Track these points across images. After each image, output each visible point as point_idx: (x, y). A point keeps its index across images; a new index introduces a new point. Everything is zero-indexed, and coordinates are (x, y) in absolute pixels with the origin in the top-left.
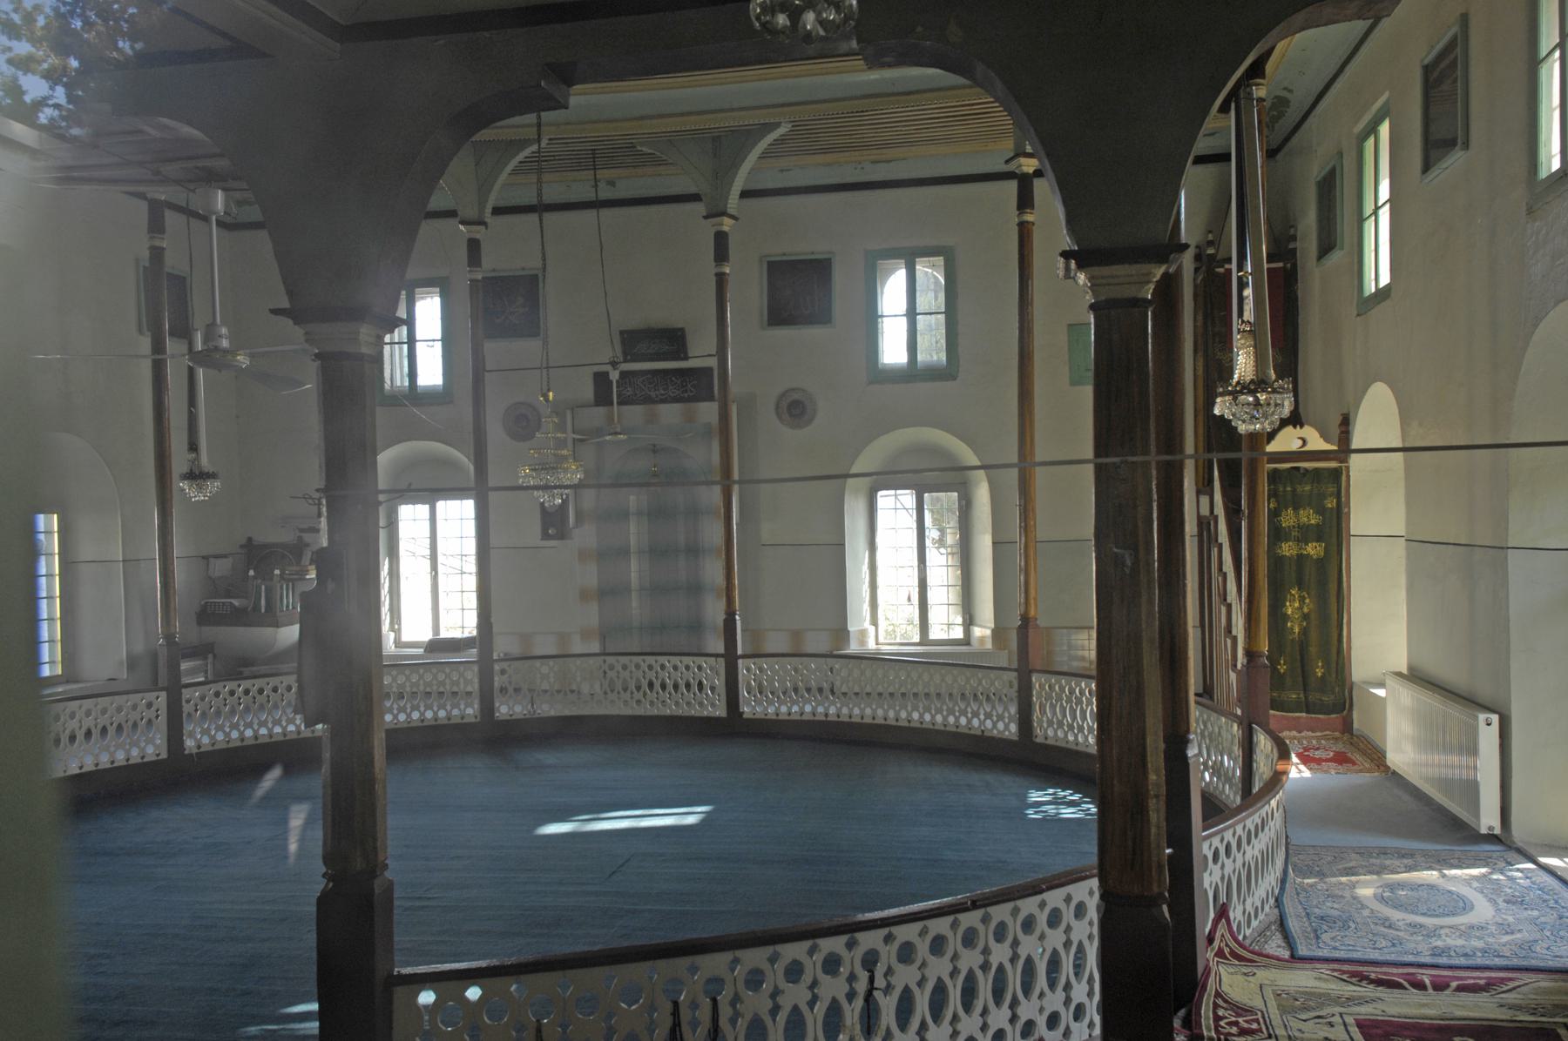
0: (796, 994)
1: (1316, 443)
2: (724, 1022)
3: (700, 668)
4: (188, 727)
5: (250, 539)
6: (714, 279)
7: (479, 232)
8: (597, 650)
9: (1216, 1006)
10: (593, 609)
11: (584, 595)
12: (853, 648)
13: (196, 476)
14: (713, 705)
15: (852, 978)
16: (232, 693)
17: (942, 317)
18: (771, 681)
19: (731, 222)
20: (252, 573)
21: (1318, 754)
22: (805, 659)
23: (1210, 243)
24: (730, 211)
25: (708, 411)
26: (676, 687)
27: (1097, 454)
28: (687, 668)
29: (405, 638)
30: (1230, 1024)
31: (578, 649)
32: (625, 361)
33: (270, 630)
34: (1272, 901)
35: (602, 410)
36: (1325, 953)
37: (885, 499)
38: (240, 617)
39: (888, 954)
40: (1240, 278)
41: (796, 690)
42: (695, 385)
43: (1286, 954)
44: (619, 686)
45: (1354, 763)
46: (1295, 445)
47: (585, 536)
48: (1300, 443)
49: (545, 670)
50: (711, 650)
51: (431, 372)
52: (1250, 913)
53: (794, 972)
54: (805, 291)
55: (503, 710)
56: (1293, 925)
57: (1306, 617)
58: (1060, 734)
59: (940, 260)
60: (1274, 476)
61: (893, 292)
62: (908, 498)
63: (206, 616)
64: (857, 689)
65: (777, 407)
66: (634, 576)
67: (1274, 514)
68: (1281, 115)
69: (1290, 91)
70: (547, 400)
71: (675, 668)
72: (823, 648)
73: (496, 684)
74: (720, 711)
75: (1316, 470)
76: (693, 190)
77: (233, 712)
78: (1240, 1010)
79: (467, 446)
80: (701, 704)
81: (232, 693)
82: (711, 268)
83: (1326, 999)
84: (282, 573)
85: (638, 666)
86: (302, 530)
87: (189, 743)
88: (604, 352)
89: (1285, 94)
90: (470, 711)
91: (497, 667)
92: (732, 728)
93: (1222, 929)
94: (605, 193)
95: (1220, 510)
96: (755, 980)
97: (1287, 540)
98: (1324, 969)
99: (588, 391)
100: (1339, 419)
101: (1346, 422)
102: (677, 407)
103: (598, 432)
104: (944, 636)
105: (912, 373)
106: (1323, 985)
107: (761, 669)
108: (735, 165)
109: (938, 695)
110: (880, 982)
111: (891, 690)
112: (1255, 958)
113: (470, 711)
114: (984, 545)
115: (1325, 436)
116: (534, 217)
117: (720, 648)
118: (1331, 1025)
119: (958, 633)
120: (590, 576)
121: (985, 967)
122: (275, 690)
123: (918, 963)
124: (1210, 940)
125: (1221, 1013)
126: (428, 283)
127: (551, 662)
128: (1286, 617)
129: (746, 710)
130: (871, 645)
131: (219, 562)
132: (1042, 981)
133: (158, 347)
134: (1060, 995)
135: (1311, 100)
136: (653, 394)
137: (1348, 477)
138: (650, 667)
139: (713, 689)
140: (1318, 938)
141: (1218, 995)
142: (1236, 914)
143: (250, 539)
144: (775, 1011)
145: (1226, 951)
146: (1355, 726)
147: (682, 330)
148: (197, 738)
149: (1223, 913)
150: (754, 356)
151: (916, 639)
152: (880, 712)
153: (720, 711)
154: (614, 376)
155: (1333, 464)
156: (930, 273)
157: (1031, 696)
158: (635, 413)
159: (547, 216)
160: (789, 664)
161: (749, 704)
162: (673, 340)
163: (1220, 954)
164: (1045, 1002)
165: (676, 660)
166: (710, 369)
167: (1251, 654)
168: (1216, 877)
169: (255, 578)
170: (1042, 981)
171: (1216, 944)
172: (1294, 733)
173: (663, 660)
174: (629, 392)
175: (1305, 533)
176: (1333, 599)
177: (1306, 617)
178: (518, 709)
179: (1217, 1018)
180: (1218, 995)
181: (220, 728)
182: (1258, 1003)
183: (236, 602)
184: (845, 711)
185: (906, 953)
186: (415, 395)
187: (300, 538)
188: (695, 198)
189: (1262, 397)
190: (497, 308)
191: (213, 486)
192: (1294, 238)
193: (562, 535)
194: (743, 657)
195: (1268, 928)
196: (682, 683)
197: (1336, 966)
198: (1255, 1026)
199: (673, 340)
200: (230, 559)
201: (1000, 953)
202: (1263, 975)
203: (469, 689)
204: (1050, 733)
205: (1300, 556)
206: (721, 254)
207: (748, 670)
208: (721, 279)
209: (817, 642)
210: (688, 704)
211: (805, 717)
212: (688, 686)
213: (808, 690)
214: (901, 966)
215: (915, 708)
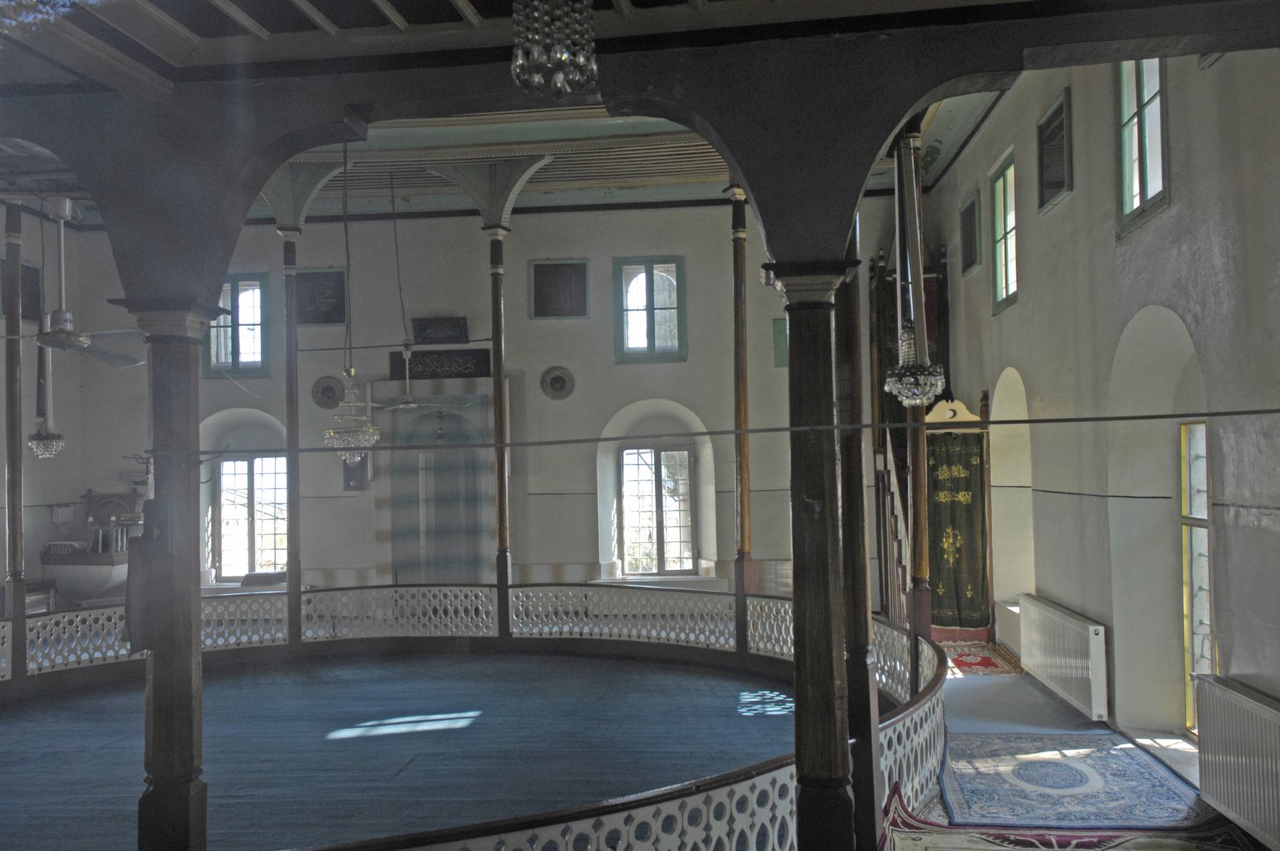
1: (965, 415)
3: (476, 596)
4: (31, 652)
5: (90, 491)
6: (490, 281)
7: (294, 237)
8: (548, 580)
10: (388, 547)
11: (380, 537)
12: (604, 578)
13: (43, 437)
14: (487, 627)
18: (535, 606)
20: (91, 519)
21: (969, 659)
22: (563, 588)
23: (881, 258)
24: (503, 224)
25: (485, 385)
26: (456, 612)
27: (793, 423)
28: (466, 596)
32: (417, 343)
33: (105, 569)
34: (934, 779)
35: (396, 383)
41: (556, 613)
42: (482, 363)
44: (419, 612)
45: (997, 666)
49: (345, 600)
51: (251, 350)
54: (558, 289)
55: (308, 634)
56: (951, 797)
57: (958, 550)
59: (673, 267)
60: (932, 440)
61: (636, 292)
62: (648, 456)
63: (47, 556)
64: (606, 612)
65: (542, 383)
67: (932, 469)
68: (934, 160)
71: (456, 597)
72: (579, 579)
74: (493, 632)
75: (964, 435)
77: (71, 638)
79: (284, 411)
80: (477, 626)
81: (71, 622)
85: (424, 596)
86: (135, 483)
87: (32, 666)
88: (398, 336)
89: (936, 144)
90: (280, 635)
91: (304, 598)
92: (503, 647)
93: (895, 803)
95: (891, 466)
97: (942, 490)
98: (975, 833)
99: (385, 368)
100: (981, 396)
101: (986, 398)
102: (458, 382)
103: (393, 401)
104: (676, 567)
105: (651, 355)
107: (527, 597)
108: (508, 189)
109: (672, 616)
111: (634, 612)
112: (922, 825)
113: (280, 635)
115: (970, 409)
116: (341, 225)
117: (494, 579)
119: (688, 565)
120: (385, 520)
122: (109, 619)
124: (886, 812)
128: (943, 551)
129: (514, 630)
130: (619, 575)
133: (12, 328)
139: (487, 613)
143: (90, 491)
145: (899, 820)
146: (997, 636)
147: (464, 318)
148: (39, 661)
149: (896, 790)
150: (527, 344)
151: (655, 570)
152: (625, 631)
153: (493, 632)
154: (407, 355)
155: (977, 431)
156: (665, 276)
159: (355, 226)
160: (551, 592)
161: (517, 626)
163: (894, 823)
165: (456, 590)
166: (487, 351)
167: (915, 580)
168: (891, 761)
169: (93, 524)
171: (891, 815)
175: (956, 485)
177: (958, 550)
181: (59, 653)
183: (76, 544)
184: (596, 630)
186: (237, 369)
187: (134, 489)
188: (474, 213)
189: (922, 379)
191: (58, 446)
192: (944, 255)
193: (361, 486)
194: (514, 586)
195: (931, 801)
196: (461, 610)
197: (984, 830)
199: (458, 327)
203: (280, 616)
204: (761, 645)
205: (953, 502)
206: (496, 258)
207: (517, 597)
208: (496, 278)
209: (574, 574)
210: (467, 627)
211: (564, 636)
212: (466, 611)
213: (567, 613)
215: (654, 627)
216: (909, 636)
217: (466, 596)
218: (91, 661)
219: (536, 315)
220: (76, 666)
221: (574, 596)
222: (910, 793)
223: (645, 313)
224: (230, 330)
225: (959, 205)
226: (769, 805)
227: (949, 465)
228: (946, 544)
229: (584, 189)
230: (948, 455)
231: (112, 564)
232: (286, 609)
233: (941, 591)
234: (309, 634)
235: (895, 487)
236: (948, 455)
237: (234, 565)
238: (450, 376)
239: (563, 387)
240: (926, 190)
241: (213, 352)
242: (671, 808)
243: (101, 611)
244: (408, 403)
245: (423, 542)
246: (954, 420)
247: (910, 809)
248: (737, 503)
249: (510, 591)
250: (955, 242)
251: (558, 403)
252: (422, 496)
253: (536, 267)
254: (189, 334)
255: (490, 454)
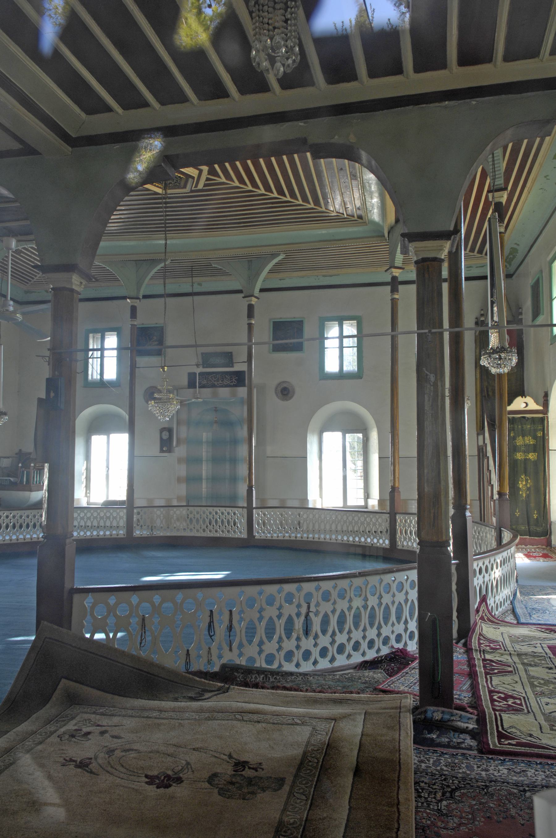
0: (271, 612)
1: (533, 406)
2: (235, 623)
3: (235, 514)
5: (20, 450)
7: (136, 303)
8: (185, 504)
9: (479, 639)
11: (179, 480)
12: (310, 506)
14: (241, 532)
15: (299, 606)
16: (7, 517)
17: (356, 349)
18: (269, 520)
19: (256, 300)
20: (20, 465)
21: (534, 554)
22: (286, 509)
23: (482, 315)
24: (255, 295)
25: (242, 391)
26: (222, 522)
27: (418, 328)
29: (92, 501)
30: (486, 646)
31: (175, 503)
33: (27, 493)
34: (509, 602)
35: (191, 390)
36: (534, 622)
37: (327, 435)
38: (14, 486)
39: (317, 597)
40: (491, 301)
42: (239, 379)
43: (515, 622)
45: (552, 558)
46: (522, 407)
47: (180, 451)
48: (525, 405)
50: (240, 505)
51: (111, 373)
52: (499, 599)
53: (270, 601)
54: (292, 336)
55: (137, 533)
56: (519, 611)
57: (528, 489)
58: (410, 544)
60: (512, 421)
65: (276, 388)
66: (204, 454)
67: (512, 439)
68: (514, 257)
69: (518, 245)
70: (164, 370)
71: (223, 513)
73: (135, 519)
74: (244, 535)
75: (533, 418)
76: (240, 288)
78: (491, 641)
79: (127, 405)
80: (235, 532)
81: (7, 517)
82: (245, 321)
83: (534, 638)
84: (35, 465)
89: (515, 246)
90: (121, 532)
91: (135, 511)
92: (250, 544)
93: (483, 607)
94: (197, 289)
95: (488, 441)
96: (251, 603)
97: (519, 452)
98: (533, 628)
100: (543, 394)
101: (546, 396)
102: (227, 389)
105: (342, 376)
106: (533, 633)
107: (264, 514)
108: (258, 274)
110: (313, 609)
112: (500, 622)
113: (121, 532)
114: (375, 459)
115: (537, 403)
118: (536, 647)
119: (362, 503)
120: (182, 470)
121: (365, 607)
122: (28, 517)
123: (332, 601)
124: (478, 611)
125: (482, 642)
126: (112, 330)
127: (162, 509)
128: (519, 489)
131: (5, 460)
132: (393, 618)
134: (402, 626)
135: (527, 249)
136: (216, 383)
137: (548, 422)
138: (210, 513)
140: (530, 616)
141: (480, 634)
142: (491, 602)
143: (20, 450)
144: (260, 619)
145: (485, 618)
146: (553, 543)
149: (484, 599)
150: (267, 368)
153: (244, 535)
155: (541, 415)
156: (350, 329)
157: (396, 525)
158: (207, 391)
160: (278, 512)
162: (229, 358)
163: (482, 618)
164: (395, 628)
165: (223, 509)
166: (244, 372)
167: (500, 494)
168: (481, 581)
169: (21, 467)
170: (393, 618)
171: (480, 613)
172: (523, 546)
173: (217, 509)
174: (205, 382)
175: (528, 449)
176: (542, 481)
177: (528, 489)
178: (145, 533)
179: (480, 644)
180: (480, 634)
182: (500, 639)
183: (12, 479)
185: (326, 597)
186: (102, 384)
188: (240, 292)
189: (503, 355)
190: (142, 342)
192: (521, 314)
193: (170, 451)
194: (256, 508)
195: (507, 612)
197: (539, 626)
198: (498, 647)
200: (11, 459)
201: (373, 601)
202: (503, 629)
204: (405, 543)
205: (526, 460)
207: (258, 514)
208: (250, 326)
212: (228, 522)
214: (324, 602)
216: (495, 529)
217: (228, 513)
218: (18, 540)
219: (273, 351)
220: (9, 542)
221: (292, 514)
222: (492, 604)
223: (338, 349)
224: (99, 359)
225: (531, 281)
226: (404, 591)
227: (523, 436)
228: (521, 485)
229: (303, 277)
230: (522, 430)
231: (31, 491)
232: (125, 517)
233: (518, 514)
234: (138, 532)
235: (490, 454)
236: (522, 430)
237: (98, 497)
238: (222, 387)
239: (287, 394)
240: (508, 276)
241: (90, 373)
242: (344, 584)
243: (24, 511)
244: (198, 398)
245: (204, 485)
246: (527, 409)
247: (493, 614)
248: (390, 464)
249: (254, 511)
250: (528, 305)
251: (285, 403)
252: (204, 458)
253: (274, 322)
254: (74, 287)
255: (243, 433)
